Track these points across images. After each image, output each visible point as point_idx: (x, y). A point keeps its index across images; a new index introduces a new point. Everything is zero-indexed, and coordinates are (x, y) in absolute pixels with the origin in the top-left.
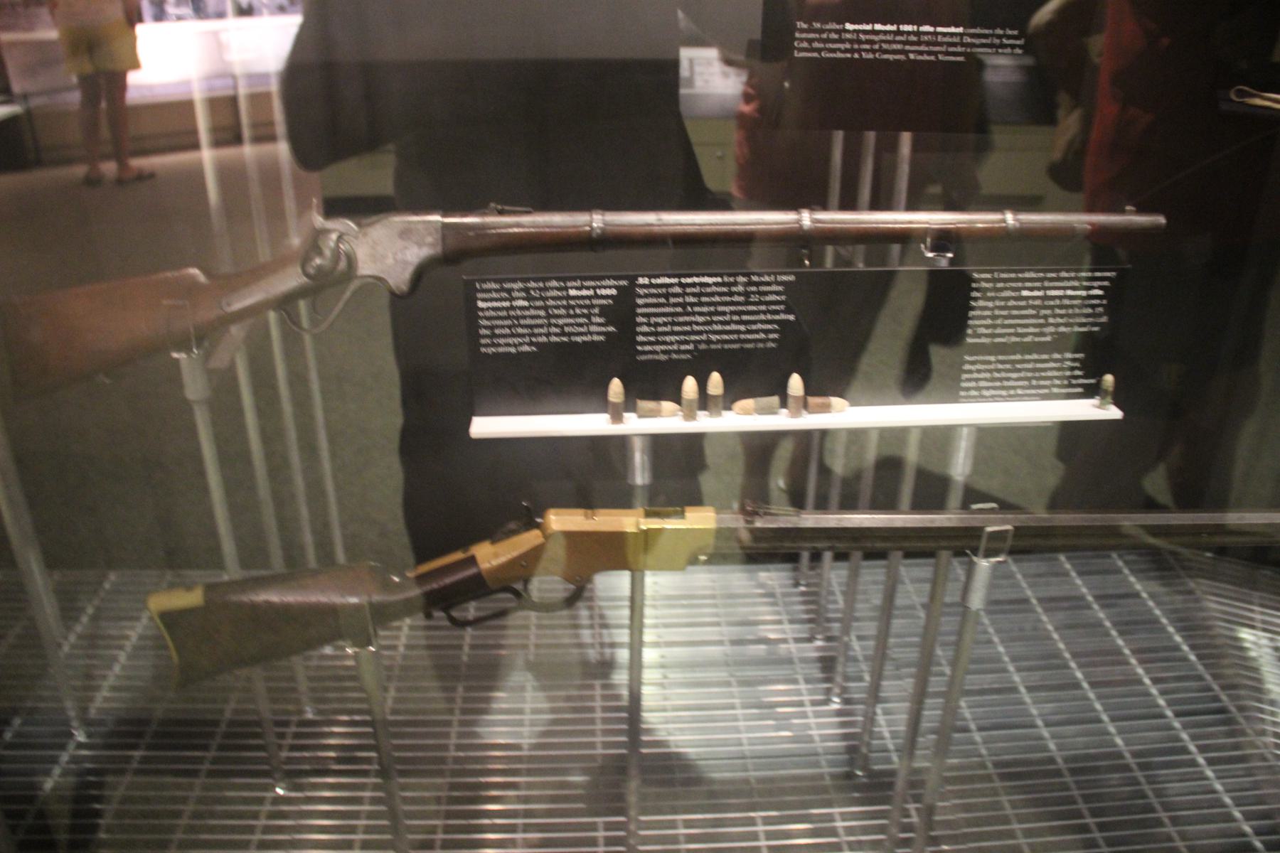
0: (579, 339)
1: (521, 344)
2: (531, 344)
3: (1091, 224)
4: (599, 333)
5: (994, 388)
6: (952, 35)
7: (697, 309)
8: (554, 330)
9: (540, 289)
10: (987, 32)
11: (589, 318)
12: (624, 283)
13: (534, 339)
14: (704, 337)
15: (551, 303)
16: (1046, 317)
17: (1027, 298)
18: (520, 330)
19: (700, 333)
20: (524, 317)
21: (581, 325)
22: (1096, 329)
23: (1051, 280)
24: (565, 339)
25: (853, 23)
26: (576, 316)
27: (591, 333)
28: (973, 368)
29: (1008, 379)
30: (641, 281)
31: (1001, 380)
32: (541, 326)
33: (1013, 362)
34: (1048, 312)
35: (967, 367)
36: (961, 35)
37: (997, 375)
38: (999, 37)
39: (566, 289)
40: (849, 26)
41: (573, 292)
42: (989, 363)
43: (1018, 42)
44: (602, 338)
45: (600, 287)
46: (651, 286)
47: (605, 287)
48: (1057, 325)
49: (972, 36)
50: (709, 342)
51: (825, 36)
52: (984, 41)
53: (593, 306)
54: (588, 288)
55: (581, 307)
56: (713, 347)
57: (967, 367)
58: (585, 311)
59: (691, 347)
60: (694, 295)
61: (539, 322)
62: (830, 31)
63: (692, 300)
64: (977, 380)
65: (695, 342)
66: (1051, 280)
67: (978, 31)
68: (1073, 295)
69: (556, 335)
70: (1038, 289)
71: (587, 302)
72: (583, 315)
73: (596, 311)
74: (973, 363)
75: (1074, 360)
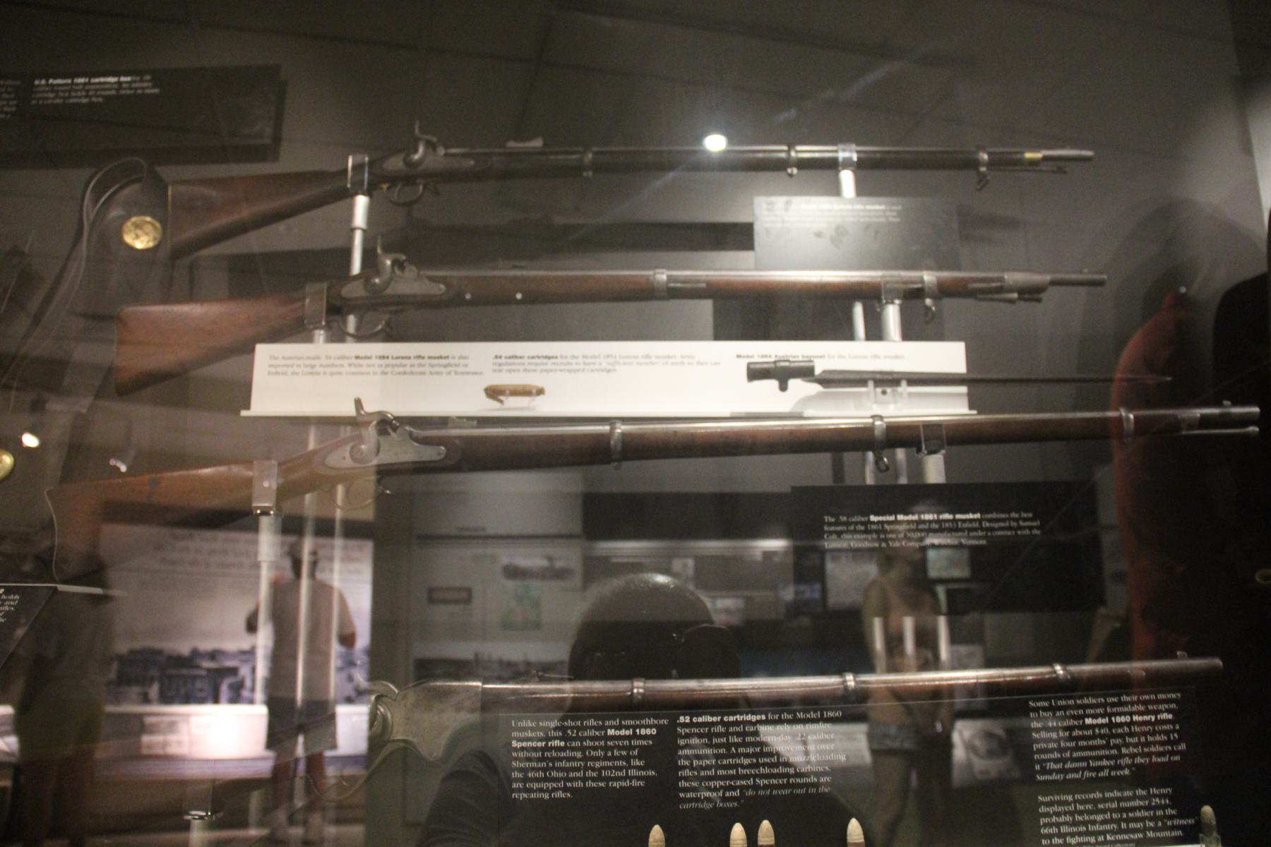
0: (616, 784)
1: (554, 790)
2: (565, 789)
3: (1146, 670)
4: (638, 778)
5: (1080, 834)
6: (971, 521)
7: (741, 750)
8: (590, 773)
9: (578, 729)
10: (1003, 516)
11: (628, 762)
12: (664, 722)
13: (569, 784)
14: (751, 782)
15: (588, 743)
16: (1118, 747)
17: (1092, 727)
18: (554, 774)
19: (747, 777)
20: (560, 759)
21: (620, 769)
22: (1177, 758)
23: (1113, 705)
24: (602, 784)
25: (876, 514)
26: (613, 758)
27: (631, 778)
28: (1050, 810)
29: (1094, 822)
30: (682, 719)
31: (1085, 823)
32: (578, 769)
33: (1095, 802)
34: (1118, 741)
35: (1043, 809)
36: (980, 521)
37: (1079, 818)
38: (1016, 520)
39: (605, 728)
40: (873, 518)
41: (611, 732)
42: (1066, 803)
43: (1035, 524)
44: (642, 783)
45: (641, 727)
46: (691, 725)
47: (646, 727)
48: (1133, 756)
49: (990, 520)
50: (756, 787)
51: (852, 528)
52: (1002, 525)
53: (634, 748)
54: (627, 728)
55: (620, 748)
56: (761, 793)
57: (1043, 809)
58: (624, 753)
59: (737, 793)
60: (738, 734)
61: (575, 764)
62: (856, 523)
63: (736, 740)
64: (1058, 825)
65: (742, 787)
66: (1113, 705)
67: (994, 516)
68: (1147, 724)
69: (593, 779)
70: (1103, 716)
71: (626, 743)
72: (621, 758)
73: (636, 753)
74: (1050, 804)
75: (1161, 796)
